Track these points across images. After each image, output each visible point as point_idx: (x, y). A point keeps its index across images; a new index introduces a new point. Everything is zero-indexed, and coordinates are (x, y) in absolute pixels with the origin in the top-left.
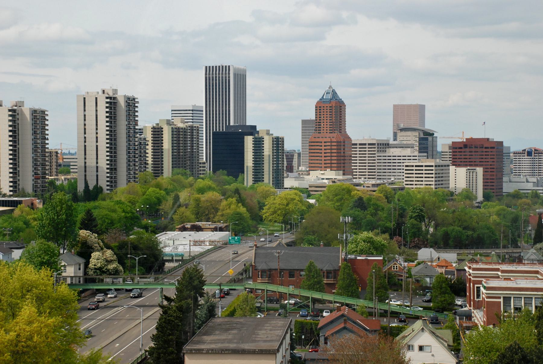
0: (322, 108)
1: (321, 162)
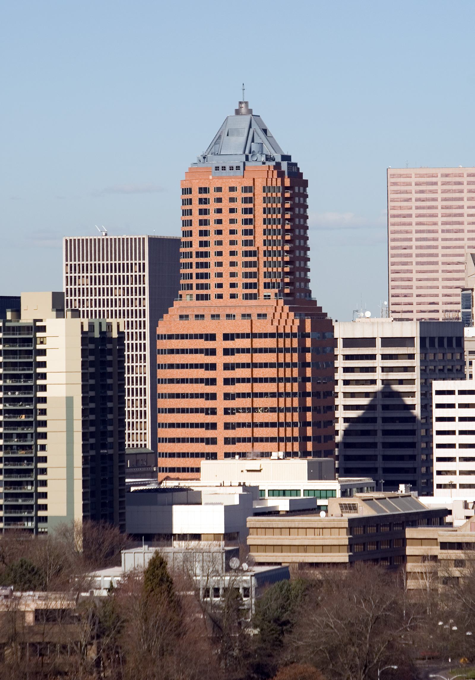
0: (212, 195)
1: (210, 359)
